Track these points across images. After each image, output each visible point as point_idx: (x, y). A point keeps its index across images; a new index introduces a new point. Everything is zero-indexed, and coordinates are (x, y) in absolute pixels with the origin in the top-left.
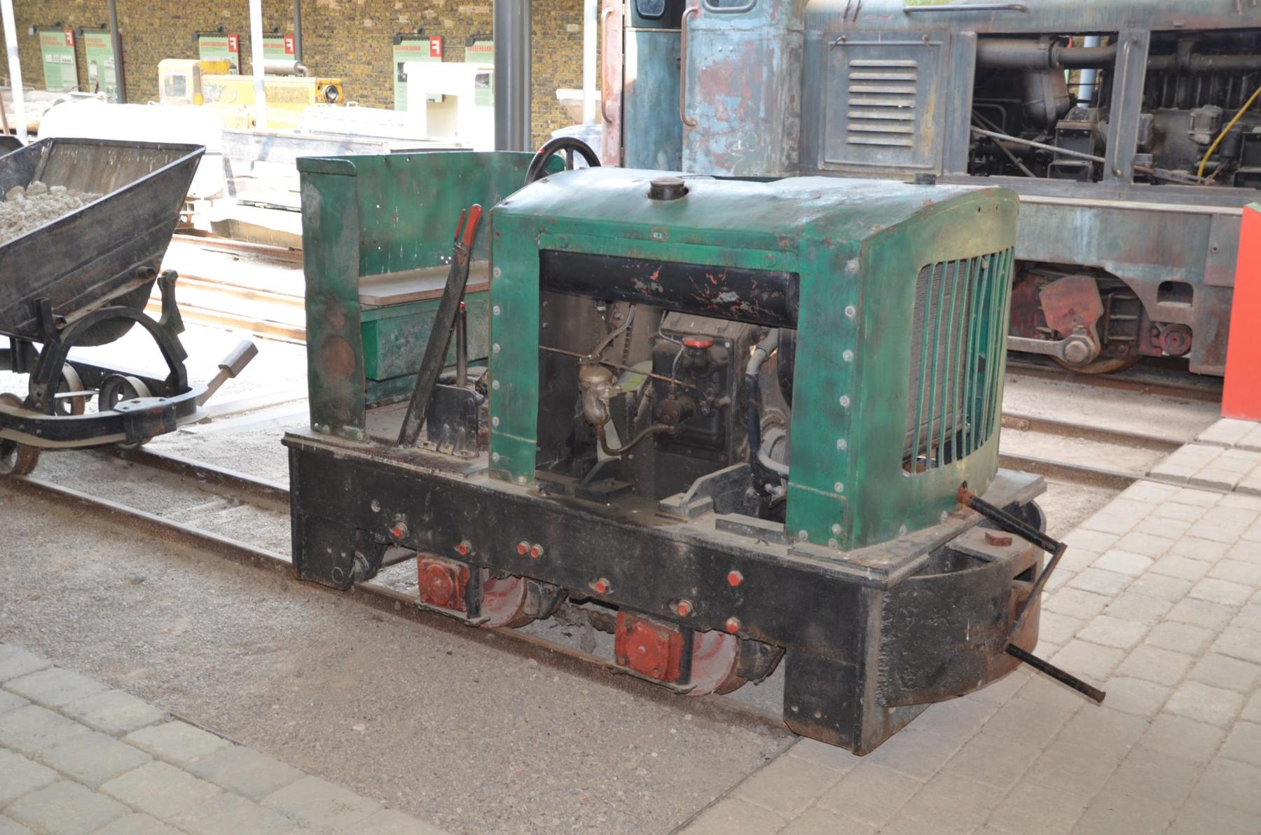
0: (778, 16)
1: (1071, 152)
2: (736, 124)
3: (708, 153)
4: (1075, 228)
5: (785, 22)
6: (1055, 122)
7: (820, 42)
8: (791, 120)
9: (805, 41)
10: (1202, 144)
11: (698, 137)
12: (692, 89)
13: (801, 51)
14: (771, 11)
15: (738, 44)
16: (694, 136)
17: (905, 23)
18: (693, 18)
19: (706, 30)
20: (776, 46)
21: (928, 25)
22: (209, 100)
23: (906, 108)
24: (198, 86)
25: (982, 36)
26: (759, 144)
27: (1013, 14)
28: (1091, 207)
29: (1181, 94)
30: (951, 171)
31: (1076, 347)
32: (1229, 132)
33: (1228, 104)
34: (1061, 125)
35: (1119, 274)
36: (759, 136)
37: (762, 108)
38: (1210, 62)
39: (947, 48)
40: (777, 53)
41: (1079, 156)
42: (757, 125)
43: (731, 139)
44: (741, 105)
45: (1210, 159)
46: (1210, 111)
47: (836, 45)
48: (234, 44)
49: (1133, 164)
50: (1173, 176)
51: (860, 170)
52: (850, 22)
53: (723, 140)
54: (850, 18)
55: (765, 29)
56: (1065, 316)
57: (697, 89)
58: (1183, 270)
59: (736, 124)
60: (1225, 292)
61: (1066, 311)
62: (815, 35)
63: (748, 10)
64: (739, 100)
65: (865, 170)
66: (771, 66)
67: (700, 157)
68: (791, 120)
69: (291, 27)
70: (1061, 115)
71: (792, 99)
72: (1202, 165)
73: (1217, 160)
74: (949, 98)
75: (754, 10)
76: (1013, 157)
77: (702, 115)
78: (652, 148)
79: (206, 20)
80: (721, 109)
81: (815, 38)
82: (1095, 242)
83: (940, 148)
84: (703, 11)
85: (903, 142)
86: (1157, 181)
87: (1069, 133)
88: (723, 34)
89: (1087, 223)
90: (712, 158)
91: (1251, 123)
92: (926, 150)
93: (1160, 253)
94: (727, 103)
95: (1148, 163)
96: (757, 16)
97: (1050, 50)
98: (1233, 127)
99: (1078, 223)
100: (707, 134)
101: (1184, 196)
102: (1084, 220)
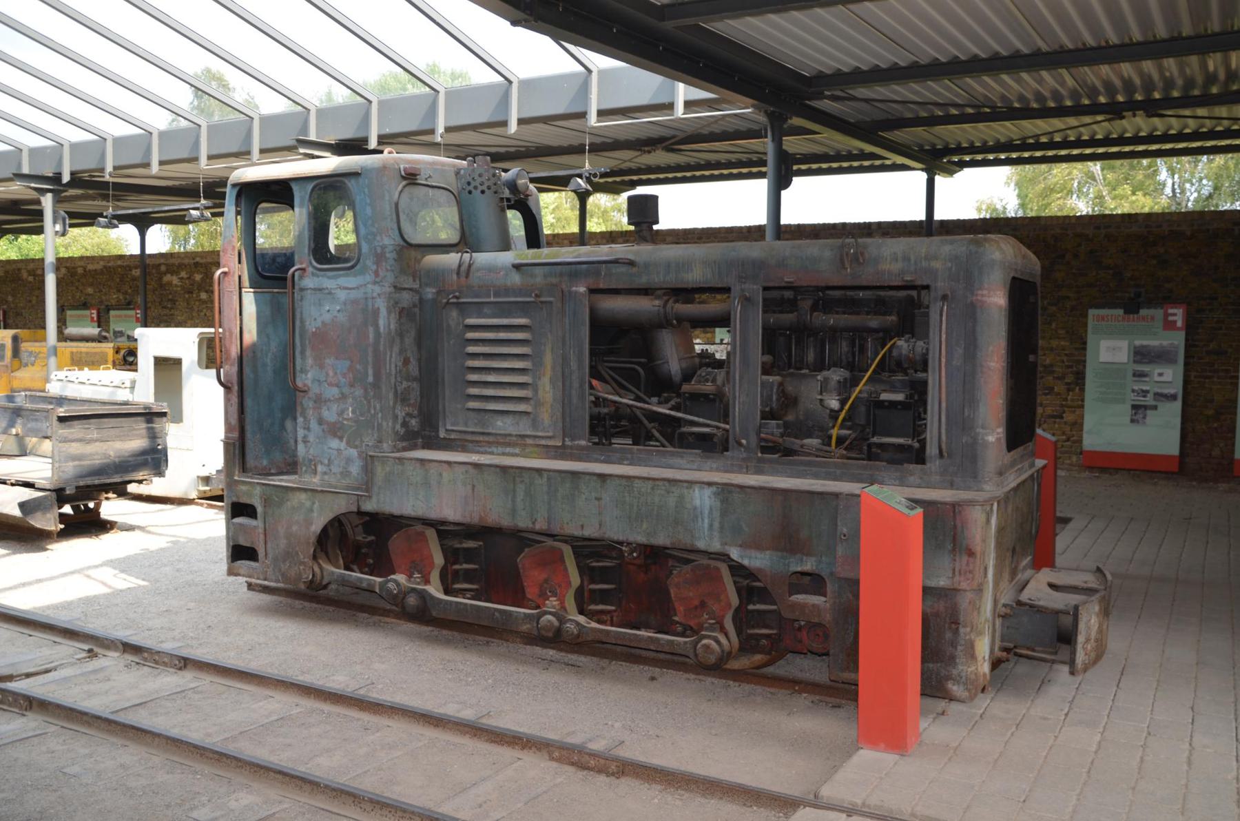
0: (381, 274)
1: (696, 419)
2: (346, 390)
3: (321, 421)
4: (695, 508)
5: (390, 278)
6: (681, 385)
7: (434, 301)
8: (405, 384)
9: (421, 300)
10: (832, 410)
11: (311, 404)
12: (303, 352)
13: (417, 310)
14: (374, 267)
15: (345, 304)
16: (308, 403)
17: (516, 279)
18: (301, 277)
19: (315, 289)
20: (382, 305)
21: (539, 280)
22: (26, 365)
23: (523, 371)
24: (16, 352)
25: (592, 291)
26: (369, 411)
27: (623, 269)
28: (710, 484)
29: (811, 356)
30: (572, 440)
31: (707, 647)
32: (857, 398)
33: (855, 369)
34: (686, 388)
35: (746, 562)
36: (369, 402)
37: (370, 372)
38: (831, 320)
39: (559, 305)
40: (383, 312)
41: (703, 425)
42: (366, 390)
43: (342, 406)
44: (351, 369)
45: (842, 427)
46: (836, 375)
47: (447, 303)
48: (95, 316)
49: (758, 433)
50: (802, 446)
51: (481, 438)
52: (463, 279)
53: (335, 407)
54: (463, 274)
55: (370, 286)
56: (696, 608)
57: (308, 353)
58: (813, 559)
59: (346, 390)
60: (854, 584)
61: (696, 602)
62: (430, 293)
63: (352, 267)
64: (347, 363)
65: (486, 438)
66: (377, 326)
67: (314, 424)
68: (405, 384)
69: (139, 300)
70: (687, 377)
71: (406, 362)
72: (834, 432)
73: (849, 429)
74: (565, 360)
75: (358, 267)
76: (646, 422)
77: (314, 380)
78: (278, 415)
79: (73, 297)
80: (331, 373)
81: (430, 296)
82: (716, 525)
83: (559, 414)
84: (310, 269)
85: (522, 407)
86: (788, 452)
87: (695, 397)
88: (330, 293)
89: (707, 502)
90: (325, 427)
91: (879, 387)
92: (545, 417)
93: (788, 539)
94: (336, 367)
95: (777, 431)
96: (362, 273)
97: (665, 306)
98: (860, 392)
99: (697, 502)
100: (319, 401)
101: (814, 469)
102: (703, 499)
